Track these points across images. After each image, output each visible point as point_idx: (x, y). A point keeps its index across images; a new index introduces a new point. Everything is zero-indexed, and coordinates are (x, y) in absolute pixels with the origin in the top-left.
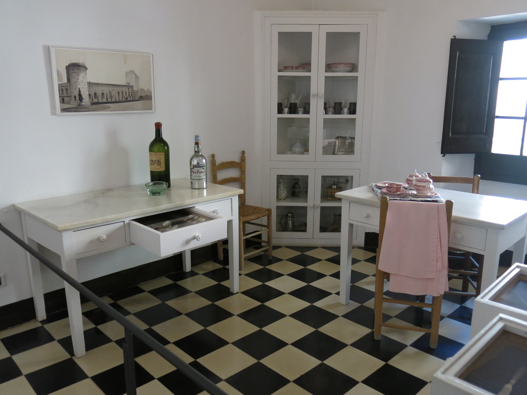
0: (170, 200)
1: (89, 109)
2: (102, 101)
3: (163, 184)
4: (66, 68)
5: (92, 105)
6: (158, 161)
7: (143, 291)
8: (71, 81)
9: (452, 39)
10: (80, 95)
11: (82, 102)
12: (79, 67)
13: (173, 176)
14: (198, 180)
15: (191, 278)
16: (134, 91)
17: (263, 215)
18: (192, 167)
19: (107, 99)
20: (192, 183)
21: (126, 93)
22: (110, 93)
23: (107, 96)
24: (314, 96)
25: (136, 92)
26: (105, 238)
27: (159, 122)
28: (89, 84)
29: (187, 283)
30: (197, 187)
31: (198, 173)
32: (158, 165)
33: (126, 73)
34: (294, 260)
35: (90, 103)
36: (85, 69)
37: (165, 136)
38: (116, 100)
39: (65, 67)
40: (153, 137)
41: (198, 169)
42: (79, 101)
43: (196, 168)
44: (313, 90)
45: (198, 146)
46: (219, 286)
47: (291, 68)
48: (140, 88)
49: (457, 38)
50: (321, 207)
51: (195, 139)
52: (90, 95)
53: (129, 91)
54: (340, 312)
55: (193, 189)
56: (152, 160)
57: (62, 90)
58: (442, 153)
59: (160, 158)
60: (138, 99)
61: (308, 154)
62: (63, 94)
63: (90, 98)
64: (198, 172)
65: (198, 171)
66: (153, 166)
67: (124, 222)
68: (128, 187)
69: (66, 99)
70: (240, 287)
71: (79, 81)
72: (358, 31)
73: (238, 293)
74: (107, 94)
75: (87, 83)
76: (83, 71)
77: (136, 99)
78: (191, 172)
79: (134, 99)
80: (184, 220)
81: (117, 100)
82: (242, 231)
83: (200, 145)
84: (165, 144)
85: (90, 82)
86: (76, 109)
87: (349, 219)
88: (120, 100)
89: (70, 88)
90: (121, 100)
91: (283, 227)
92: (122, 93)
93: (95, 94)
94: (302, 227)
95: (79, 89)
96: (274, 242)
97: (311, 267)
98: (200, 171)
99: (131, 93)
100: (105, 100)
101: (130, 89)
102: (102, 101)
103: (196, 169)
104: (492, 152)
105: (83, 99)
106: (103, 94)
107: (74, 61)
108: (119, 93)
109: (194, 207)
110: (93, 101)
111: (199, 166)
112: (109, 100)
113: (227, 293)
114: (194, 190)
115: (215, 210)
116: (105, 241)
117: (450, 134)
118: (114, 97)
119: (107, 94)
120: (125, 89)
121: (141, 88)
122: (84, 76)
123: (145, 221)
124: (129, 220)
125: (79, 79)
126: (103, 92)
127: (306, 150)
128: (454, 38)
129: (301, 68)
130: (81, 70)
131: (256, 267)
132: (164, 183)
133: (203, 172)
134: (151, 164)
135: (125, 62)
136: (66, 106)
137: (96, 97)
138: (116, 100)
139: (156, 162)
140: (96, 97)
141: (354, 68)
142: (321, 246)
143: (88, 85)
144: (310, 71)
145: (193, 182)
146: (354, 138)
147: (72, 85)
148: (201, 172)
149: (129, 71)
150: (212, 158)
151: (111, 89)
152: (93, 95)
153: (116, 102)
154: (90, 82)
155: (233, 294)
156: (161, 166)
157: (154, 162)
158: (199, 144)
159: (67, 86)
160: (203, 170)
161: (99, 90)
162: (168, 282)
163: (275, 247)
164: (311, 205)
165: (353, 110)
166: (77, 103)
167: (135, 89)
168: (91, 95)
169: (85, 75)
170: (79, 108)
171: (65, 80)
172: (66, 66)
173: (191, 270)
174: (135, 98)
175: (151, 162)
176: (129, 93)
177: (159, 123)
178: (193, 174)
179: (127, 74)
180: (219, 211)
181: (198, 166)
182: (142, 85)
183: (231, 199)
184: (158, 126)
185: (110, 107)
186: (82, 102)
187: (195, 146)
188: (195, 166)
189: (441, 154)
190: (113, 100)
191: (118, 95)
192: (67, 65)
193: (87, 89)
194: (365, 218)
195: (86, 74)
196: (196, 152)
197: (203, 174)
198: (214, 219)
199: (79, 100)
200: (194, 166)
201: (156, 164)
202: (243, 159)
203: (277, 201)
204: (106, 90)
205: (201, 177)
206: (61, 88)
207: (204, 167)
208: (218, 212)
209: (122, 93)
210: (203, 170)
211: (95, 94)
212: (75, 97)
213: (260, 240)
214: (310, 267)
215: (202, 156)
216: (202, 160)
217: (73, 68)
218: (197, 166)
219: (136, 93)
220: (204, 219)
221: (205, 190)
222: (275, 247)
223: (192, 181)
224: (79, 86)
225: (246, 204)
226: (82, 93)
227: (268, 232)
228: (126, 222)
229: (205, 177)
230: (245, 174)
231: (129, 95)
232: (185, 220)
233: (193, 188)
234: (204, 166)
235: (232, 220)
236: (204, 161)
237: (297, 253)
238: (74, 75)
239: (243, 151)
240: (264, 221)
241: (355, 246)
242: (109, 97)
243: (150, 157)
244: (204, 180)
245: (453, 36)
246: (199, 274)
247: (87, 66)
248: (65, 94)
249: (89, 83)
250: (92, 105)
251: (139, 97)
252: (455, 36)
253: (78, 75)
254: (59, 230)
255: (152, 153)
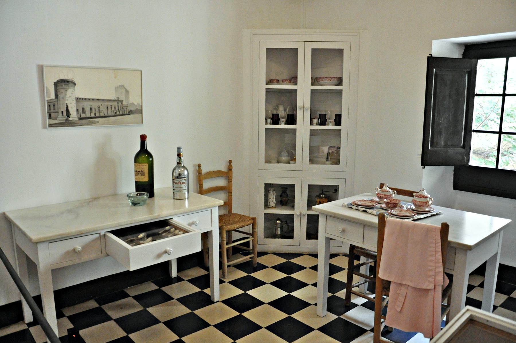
0: (151, 210)
1: (75, 124)
2: (90, 116)
3: (143, 194)
4: (54, 84)
5: (79, 120)
6: (142, 172)
7: (128, 296)
8: (59, 97)
9: (428, 57)
10: (67, 110)
11: (70, 118)
12: (67, 82)
13: (157, 186)
14: (179, 191)
15: (177, 284)
16: (124, 106)
17: (247, 223)
18: (174, 178)
19: (95, 114)
20: (174, 193)
21: (115, 107)
22: (98, 108)
23: (95, 111)
24: (300, 108)
25: (126, 107)
26: (79, 250)
27: (144, 134)
28: (77, 100)
29: (171, 290)
30: (178, 198)
31: (180, 184)
32: (142, 176)
33: (116, 88)
34: (279, 268)
35: (77, 118)
36: (73, 85)
37: (149, 148)
38: (104, 114)
39: (54, 83)
40: (138, 148)
41: (179, 180)
42: (66, 117)
43: (177, 179)
44: (299, 103)
45: (180, 158)
46: (201, 293)
47: (276, 81)
48: (131, 102)
49: (433, 55)
50: (308, 215)
51: (177, 151)
52: (77, 110)
53: (118, 105)
54: (316, 323)
55: (175, 199)
56: (136, 170)
57: (50, 106)
58: (422, 165)
59: (144, 169)
60: (127, 113)
61: (295, 163)
62: (50, 110)
63: (78, 113)
64: (179, 183)
65: (179, 182)
66: (137, 177)
67: (100, 233)
68: (115, 195)
69: (53, 115)
70: (221, 295)
71: (67, 96)
72: (342, 48)
73: (218, 301)
74: (95, 109)
75: (75, 98)
76: (72, 87)
77: (126, 113)
78: (173, 182)
79: (123, 113)
80: (160, 232)
81: (106, 114)
82: (225, 239)
83: (183, 156)
84: (150, 155)
85: (78, 97)
86: (61, 124)
87: (326, 233)
88: (109, 114)
89: (58, 103)
90: (109, 114)
91: (271, 234)
92: (111, 107)
93: (83, 109)
94: (288, 234)
95: (67, 104)
96: (259, 248)
97: (294, 276)
98: (181, 182)
99: (121, 107)
100: (93, 115)
101: (120, 104)
102: (90, 116)
103: (178, 180)
104: (470, 165)
105: (70, 115)
106: (91, 109)
107: (62, 77)
108: (107, 107)
109: (172, 218)
110: (80, 116)
111: (180, 177)
112: (98, 115)
113: (208, 301)
114: (175, 200)
115: (194, 221)
116: (79, 252)
117: (430, 147)
118: (103, 112)
119: (95, 109)
120: (115, 104)
121: (131, 102)
122: (73, 91)
123: (120, 233)
124: (105, 232)
125: (67, 95)
126: (91, 107)
127: (292, 158)
128: (430, 56)
129: (287, 81)
130: (70, 86)
131: (242, 274)
132: (146, 194)
133: (185, 183)
134: (136, 175)
135: (115, 77)
136: (53, 122)
137: (83, 112)
138: (104, 114)
139: (140, 172)
140: (83, 112)
141: (340, 82)
142: (308, 253)
143: (76, 100)
144: (296, 84)
145: (175, 192)
146: (340, 148)
147: (60, 101)
148: (182, 183)
149: (119, 86)
150: (197, 168)
151: (99, 103)
152: (80, 110)
153: (104, 117)
154: (78, 97)
155: (213, 302)
156: (145, 176)
157: (138, 172)
158: (182, 155)
159: (55, 102)
160: (184, 181)
161: (87, 106)
162: (153, 287)
163: (261, 254)
164: (298, 213)
165: (338, 121)
166: (64, 119)
167: (124, 103)
168: (79, 110)
169: (74, 90)
170: (67, 123)
171: (53, 96)
172: (55, 83)
173: (177, 275)
174: (124, 112)
175: (136, 172)
176: (118, 107)
177: (145, 135)
178: (175, 185)
179: (117, 89)
180: (197, 223)
181: (180, 176)
182: (134, 100)
183: (211, 210)
184: (143, 138)
185: (98, 122)
186: (70, 118)
187: (177, 158)
188: (176, 178)
189: (421, 166)
190: (102, 114)
191: (106, 109)
192: (56, 81)
193: (75, 105)
194: (340, 232)
195: (75, 90)
196: (178, 163)
197: (185, 184)
198: (188, 232)
199: (67, 115)
200: (176, 177)
201: (140, 174)
202: (230, 169)
203: (265, 209)
204: (95, 105)
205: (182, 187)
206: (48, 104)
207: (185, 178)
208: (197, 224)
209: (111, 107)
210: (184, 181)
211: (83, 109)
212: (62, 112)
213: (231, 254)
214: (293, 276)
215: (184, 167)
216: (184, 171)
217: (61, 84)
218: (178, 177)
219: (125, 107)
220: (181, 232)
221: (187, 200)
222: (261, 254)
223: (174, 192)
224: (67, 102)
225: (233, 212)
226: (69, 108)
227: (253, 240)
228: (101, 234)
229: (186, 188)
230: (232, 183)
231: (118, 109)
232: (160, 232)
233: (175, 198)
234: (185, 177)
235: (212, 230)
236: (186, 172)
237: (283, 260)
238: (62, 91)
239: (230, 160)
240: (249, 229)
241: (341, 253)
242: (98, 112)
243: (135, 168)
244: (185, 190)
245: (429, 54)
246: (184, 280)
247: (75, 82)
248: (52, 110)
249: (78, 99)
250: (79, 120)
251: (128, 111)
252: (431, 55)
253: (66, 91)
254: (33, 242)
255: (136, 164)
